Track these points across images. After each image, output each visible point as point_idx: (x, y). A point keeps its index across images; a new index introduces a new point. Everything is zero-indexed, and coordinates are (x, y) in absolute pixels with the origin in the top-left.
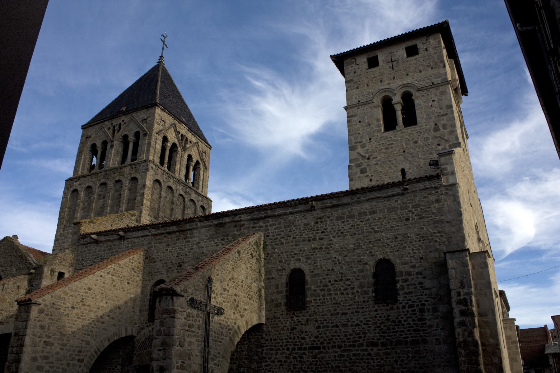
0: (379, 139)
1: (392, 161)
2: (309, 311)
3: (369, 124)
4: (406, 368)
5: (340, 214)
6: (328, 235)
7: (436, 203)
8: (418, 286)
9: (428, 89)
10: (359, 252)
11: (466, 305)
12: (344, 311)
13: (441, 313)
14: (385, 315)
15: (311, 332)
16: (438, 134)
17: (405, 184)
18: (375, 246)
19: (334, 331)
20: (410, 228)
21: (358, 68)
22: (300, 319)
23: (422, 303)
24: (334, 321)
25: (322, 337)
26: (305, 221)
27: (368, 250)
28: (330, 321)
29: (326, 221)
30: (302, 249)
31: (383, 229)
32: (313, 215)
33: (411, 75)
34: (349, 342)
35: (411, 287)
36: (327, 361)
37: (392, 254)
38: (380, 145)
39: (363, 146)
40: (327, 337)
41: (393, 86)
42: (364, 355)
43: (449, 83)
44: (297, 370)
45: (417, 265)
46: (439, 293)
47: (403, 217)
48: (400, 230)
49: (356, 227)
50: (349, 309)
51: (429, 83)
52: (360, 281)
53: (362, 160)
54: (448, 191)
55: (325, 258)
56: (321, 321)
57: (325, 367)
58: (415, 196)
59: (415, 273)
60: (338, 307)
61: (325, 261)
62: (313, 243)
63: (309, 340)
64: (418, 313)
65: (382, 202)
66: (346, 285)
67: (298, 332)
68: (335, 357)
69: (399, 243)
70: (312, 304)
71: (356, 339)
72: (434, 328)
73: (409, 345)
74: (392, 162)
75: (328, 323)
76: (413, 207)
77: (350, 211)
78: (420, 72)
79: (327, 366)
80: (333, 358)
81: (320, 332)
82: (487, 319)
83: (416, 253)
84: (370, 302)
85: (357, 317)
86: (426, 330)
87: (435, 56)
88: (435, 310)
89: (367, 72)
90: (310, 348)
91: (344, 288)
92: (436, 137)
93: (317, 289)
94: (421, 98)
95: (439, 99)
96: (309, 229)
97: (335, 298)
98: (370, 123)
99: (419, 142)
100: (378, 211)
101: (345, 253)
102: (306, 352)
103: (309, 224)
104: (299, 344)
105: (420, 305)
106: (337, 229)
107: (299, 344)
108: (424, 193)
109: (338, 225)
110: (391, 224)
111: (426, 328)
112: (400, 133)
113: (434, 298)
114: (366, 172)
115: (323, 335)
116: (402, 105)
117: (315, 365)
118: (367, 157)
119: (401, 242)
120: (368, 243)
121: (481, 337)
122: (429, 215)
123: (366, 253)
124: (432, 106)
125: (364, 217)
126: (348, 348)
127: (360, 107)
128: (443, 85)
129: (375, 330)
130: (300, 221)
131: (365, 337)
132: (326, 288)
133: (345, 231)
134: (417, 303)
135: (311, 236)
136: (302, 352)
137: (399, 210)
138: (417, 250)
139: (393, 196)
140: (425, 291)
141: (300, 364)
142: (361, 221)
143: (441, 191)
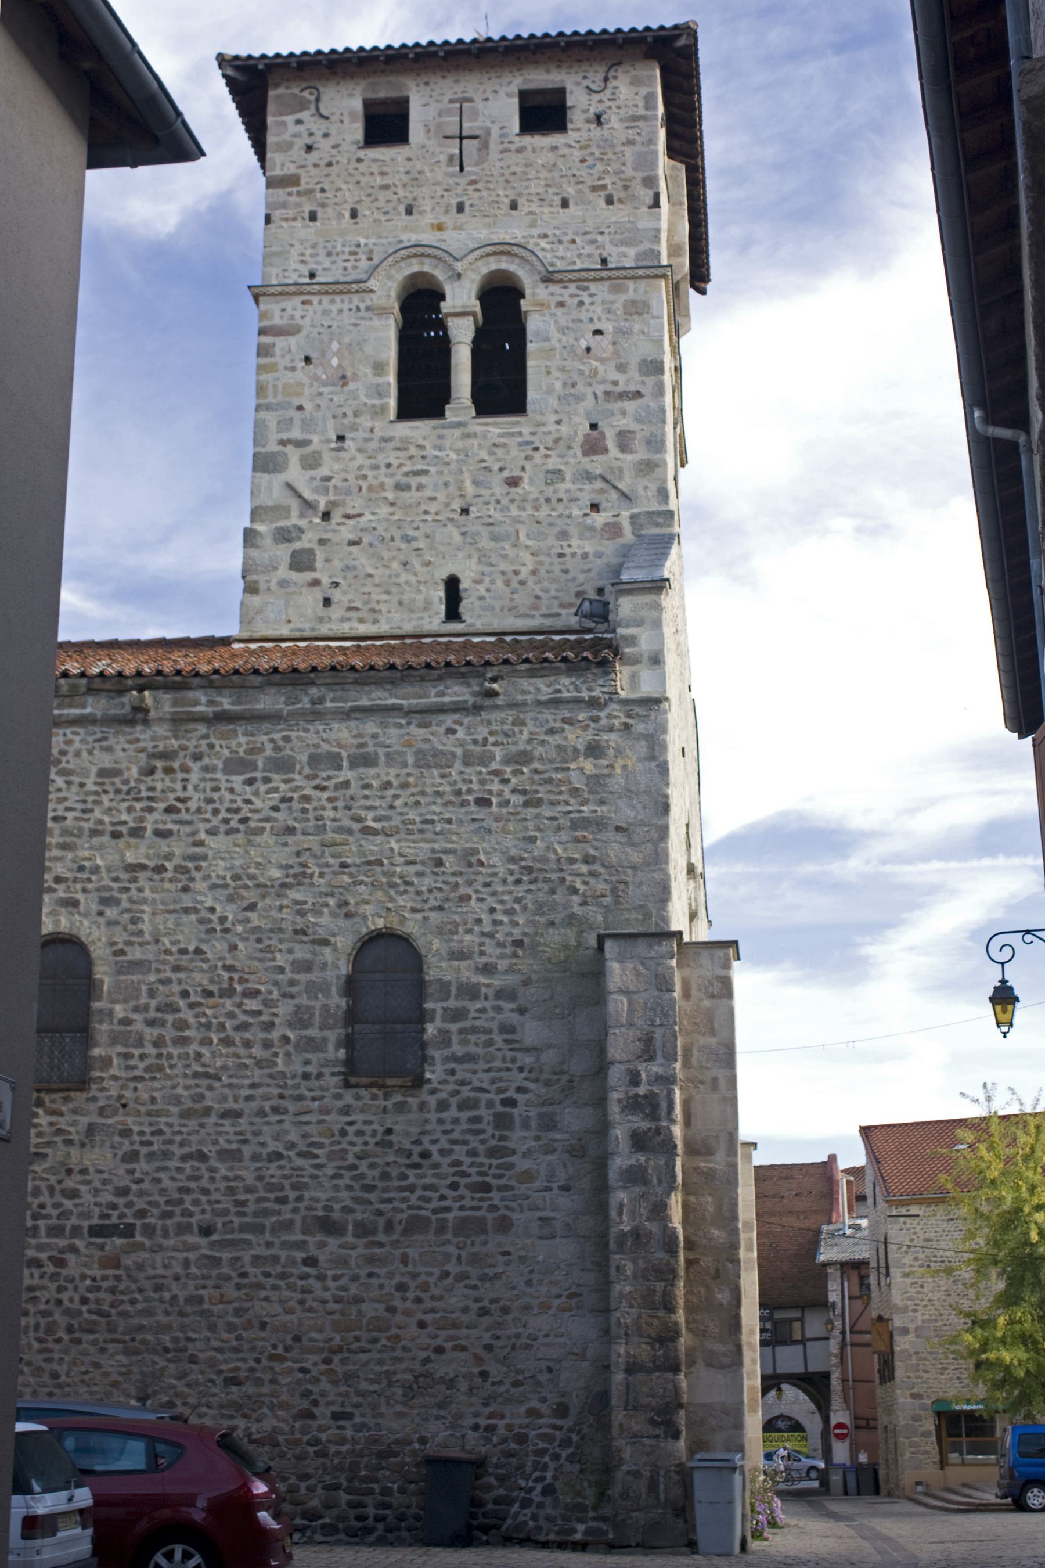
0: (373, 445)
1: (415, 539)
2: (99, 1095)
3: (344, 377)
4: (433, 1311)
5: (241, 751)
6: (189, 823)
7: (587, 757)
8: (498, 1039)
9: (587, 280)
10: (299, 897)
11: (654, 1116)
12: (231, 1105)
13: (566, 1136)
14: (375, 1127)
15: (101, 1172)
16: (597, 465)
17: (489, 675)
18: (362, 883)
19: (188, 1171)
20: (489, 831)
21: (326, 135)
22: (62, 1123)
23: (508, 1095)
24: (194, 1138)
25: (141, 1194)
26: (106, 761)
27: (332, 895)
28: (178, 1138)
29: (185, 769)
30: (87, 864)
31: (393, 823)
32: (138, 740)
33: (527, 209)
34: (244, 1214)
35: (472, 1038)
36: (154, 1277)
37: (419, 916)
38: (376, 467)
39: (311, 462)
40: (163, 1191)
41: (454, 240)
42: (293, 1262)
43: (664, 276)
44: (42, 1307)
45: (502, 965)
46: (565, 1067)
47: (469, 791)
48: (455, 838)
49: (296, 805)
50: (249, 1098)
51: (589, 256)
52: (297, 1001)
53: (302, 515)
54: (630, 721)
55: (171, 907)
56: (142, 1133)
57: (147, 1300)
58: (519, 723)
59: (490, 992)
60: (210, 1088)
61: (171, 918)
62: (129, 846)
63: (93, 1200)
64: (490, 1130)
65: (401, 726)
66: (245, 1012)
67: (52, 1171)
68: (186, 1264)
69: (445, 882)
70: (113, 1071)
71: (267, 1205)
72: (537, 1184)
73: (449, 1236)
74: (415, 545)
75: (170, 1142)
76: (507, 761)
77: (281, 743)
78: (565, 204)
79: (156, 1296)
80: (179, 1270)
81: (137, 1175)
82: (711, 1165)
83: (501, 923)
84: (327, 1077)
85: (277, 1128)
86: (512, 1188)
87: (628, 151)
88: (548, 1123)
89: (359, 160)
90: (95, 1231)
91: (236, 1022)
92: (589, 477)
93: (135, 1016)
94: (553, 310)
95: (620, 331)
96: (118, 791)
97: (199, 1055)
98: (349, 374)
99: (525, 484)
100: (382, 759)
101: (251, 896)
102: (79, 1243)
103: (117, 773)
104: (55, 1213)
105: (498, 1103)
106: (226, 805)
107: (55, 1213)
108: (550, 717)
109: (231, 790)
110: (423, 810)
111: (513, 1183)
112: (457, 432)
113: (547, 1083)
114: (312, 568)
115: (146, 1185)
116: (476, 321)
117: (112, 1291)
118: (322, 507)
119: (452, 879)
120: (337, 868)
121: (685, 1221)
122: (561, 797)
123: (327, 905)
124: (588, 350)
125: (331, 773)
126: (236, 1236)
127: (315, 299)
128: (641, 277)
129: (336, 1176)
130: (85, 754)
131: (300, 1199)
132: (170, 1018)
133: (256, 816)
134: (488, 1096)
135: (124, 817)
136: (63, 1243)
137: (458, 765)
138: (506, 912)
139: (441, 710)
140: (519, 1055)
141: (53, 1286)
142: (316, 788)
143: (610, 716)
